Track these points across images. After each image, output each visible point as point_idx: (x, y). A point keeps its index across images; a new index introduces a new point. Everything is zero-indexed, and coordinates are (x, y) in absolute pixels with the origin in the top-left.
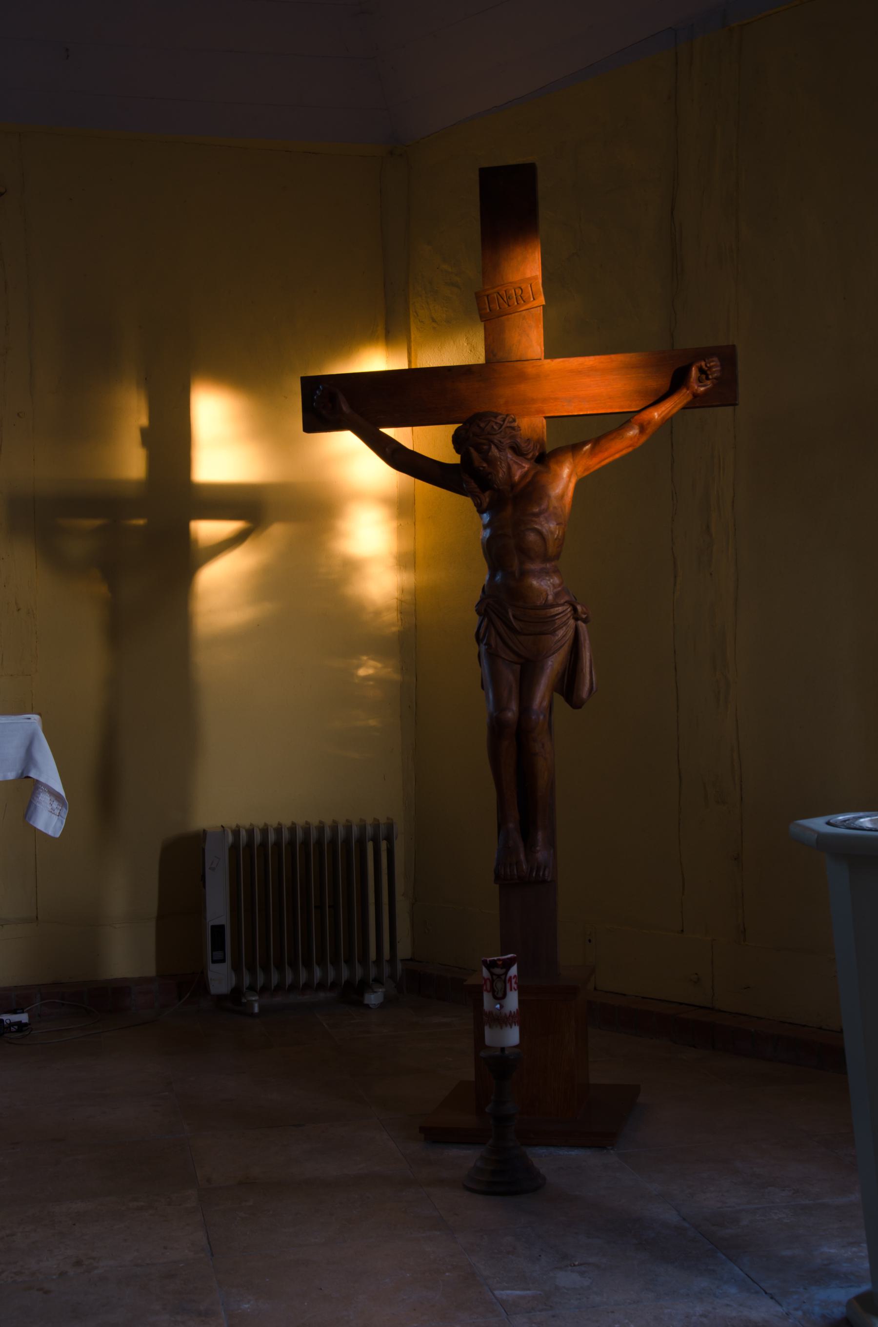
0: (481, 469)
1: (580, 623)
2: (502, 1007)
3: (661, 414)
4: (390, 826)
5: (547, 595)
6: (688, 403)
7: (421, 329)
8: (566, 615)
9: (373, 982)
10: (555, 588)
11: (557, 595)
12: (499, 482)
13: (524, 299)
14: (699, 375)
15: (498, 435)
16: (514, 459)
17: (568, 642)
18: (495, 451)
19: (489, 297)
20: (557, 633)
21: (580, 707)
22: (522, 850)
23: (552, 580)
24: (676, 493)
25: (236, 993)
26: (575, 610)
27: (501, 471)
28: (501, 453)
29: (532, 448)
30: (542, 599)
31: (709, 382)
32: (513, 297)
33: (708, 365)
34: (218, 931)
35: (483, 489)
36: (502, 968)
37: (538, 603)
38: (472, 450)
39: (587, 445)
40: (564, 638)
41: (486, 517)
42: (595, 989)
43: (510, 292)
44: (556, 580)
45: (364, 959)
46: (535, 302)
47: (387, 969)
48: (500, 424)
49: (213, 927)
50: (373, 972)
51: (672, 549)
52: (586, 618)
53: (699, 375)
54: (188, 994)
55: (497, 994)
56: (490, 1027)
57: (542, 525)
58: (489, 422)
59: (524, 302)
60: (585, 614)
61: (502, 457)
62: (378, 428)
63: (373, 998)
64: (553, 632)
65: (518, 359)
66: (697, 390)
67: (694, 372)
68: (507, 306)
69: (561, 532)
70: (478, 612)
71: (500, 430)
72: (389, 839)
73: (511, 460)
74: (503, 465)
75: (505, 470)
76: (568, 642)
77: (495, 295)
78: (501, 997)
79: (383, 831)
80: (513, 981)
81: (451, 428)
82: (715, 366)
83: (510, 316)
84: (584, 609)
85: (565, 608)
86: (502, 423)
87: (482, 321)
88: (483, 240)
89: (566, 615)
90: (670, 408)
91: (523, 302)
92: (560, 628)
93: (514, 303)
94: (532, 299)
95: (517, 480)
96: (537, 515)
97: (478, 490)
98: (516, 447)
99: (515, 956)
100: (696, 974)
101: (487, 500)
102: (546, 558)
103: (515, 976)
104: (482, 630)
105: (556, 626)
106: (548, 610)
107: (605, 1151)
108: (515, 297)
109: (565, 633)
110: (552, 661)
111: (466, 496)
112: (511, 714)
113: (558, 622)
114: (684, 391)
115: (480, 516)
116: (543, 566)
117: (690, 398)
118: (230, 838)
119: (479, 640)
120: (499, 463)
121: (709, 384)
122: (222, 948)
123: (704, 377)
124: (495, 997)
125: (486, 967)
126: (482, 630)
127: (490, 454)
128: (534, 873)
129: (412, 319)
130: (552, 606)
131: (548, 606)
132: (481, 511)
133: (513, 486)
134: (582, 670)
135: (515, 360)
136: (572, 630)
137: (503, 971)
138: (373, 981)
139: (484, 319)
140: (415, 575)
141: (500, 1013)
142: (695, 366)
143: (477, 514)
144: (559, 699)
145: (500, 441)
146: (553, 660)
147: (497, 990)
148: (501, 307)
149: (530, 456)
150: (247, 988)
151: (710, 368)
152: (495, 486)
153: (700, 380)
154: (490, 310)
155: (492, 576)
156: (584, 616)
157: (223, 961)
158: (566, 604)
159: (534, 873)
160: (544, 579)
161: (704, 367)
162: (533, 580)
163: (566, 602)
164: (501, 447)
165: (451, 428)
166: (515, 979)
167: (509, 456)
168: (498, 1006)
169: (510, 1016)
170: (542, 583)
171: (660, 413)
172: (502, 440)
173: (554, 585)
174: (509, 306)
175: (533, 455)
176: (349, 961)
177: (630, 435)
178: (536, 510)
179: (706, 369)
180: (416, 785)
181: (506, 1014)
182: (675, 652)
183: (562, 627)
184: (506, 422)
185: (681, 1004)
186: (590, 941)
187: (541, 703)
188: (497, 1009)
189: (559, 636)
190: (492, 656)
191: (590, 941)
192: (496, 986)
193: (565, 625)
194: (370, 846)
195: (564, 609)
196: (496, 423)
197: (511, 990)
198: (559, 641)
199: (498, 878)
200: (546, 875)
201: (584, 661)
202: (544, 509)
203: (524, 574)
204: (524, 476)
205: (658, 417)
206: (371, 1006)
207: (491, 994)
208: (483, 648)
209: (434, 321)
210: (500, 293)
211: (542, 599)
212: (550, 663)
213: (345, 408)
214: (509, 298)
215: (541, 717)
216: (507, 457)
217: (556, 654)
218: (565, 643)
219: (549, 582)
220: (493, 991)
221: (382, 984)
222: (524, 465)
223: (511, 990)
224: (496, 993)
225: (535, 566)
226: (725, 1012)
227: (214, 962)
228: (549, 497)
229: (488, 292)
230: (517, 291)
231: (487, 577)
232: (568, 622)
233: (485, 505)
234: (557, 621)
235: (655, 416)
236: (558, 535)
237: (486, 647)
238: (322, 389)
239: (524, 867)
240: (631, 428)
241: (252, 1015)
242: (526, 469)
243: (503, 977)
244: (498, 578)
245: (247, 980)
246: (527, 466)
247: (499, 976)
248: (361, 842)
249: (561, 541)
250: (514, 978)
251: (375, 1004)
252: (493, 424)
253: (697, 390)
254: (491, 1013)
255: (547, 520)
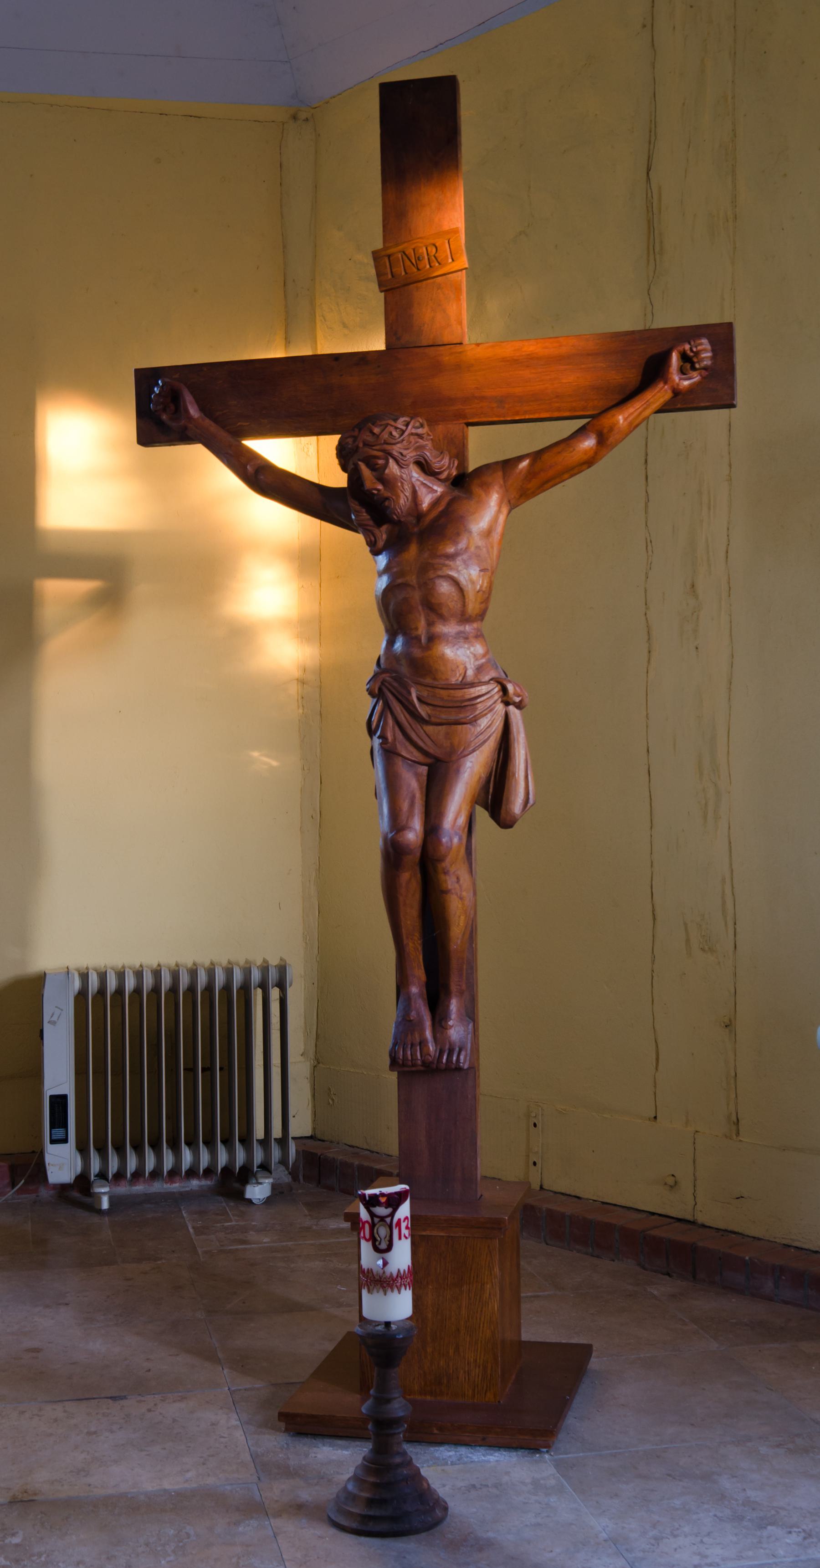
0: (375, 492)
1: (511, 708)
2: (385, 1263)
3: (627, 418)
4: (282, 969)
5: (466, 670)
6: (667, 403)
7: (329, 337)
8: (492, 697)
9: (259, 1169)
10: (477, 660)
11: (479, 669)
12: (399, 510)
13: (439, 260)
14: (682, 364)
15: (399, 445)
16: (421, 479)
17: (494, 735)
18: (393, 467)
19: (391, 259)
20: (479, 722)
21: (510, 826)
22: (428, 1023)
23: (472, 649)
24: (651, 542)
25: (83, 1182)
26: (504, 690)
27: (402, 495)
28: (403, 471)
29: (447, 464)
30: (458, 675)
31: (695, 374)
32: (423, 258)
33: (695, 349)
34: (59, 1102)
35: (379, 524)
36: (386, 1208)
37: (453, 681)
38: (363, 466)
39: (524, 461)
40: (489, 729)
41: (382, 560)
42: (541, 1187)
43: (420, 251)
44: (479, 649)
45: (246, 1140)
46: (454, 264)
47: (276, 1153)
48: (401, 430)
49: (51, 1097)
50: (258, 1156)
51: (646, 614)
52: (521, 701)
53: (682, 364)
54: (23, 1181)
55: (380, 1244)
56: (369, 1291)
57: (458, 571)
58: (386, 427)
59: (440, 264)
60: (518, 696)
61: (404, 476)
62: (239, 439)
63: (258, 1191)
64: (474, 721)
65: (431, 343)
66: (678, 385)
67: (675, 358)
68: (415, 270)
69: (485, 581)
70: (371, 693)
71: (402, 438)
72: (281, 985)
73: (418, 480)
74: (406, 487)
75: (407, 494)
76: (494, 735)
77: (400, 256)
78: (383, 1249)
79: (273, 976)
80: (403, 1225)
81: (334, 439)
82: (705, 350)
83: (419, 284)
84: (517, 689)
85: (490, 687)
86: (404, 428)
87: (381, 291)
88: (384, 181)
89: (492, 697)
90: (640, 410)
91: (437, 264)
92: (482, 715)
93: (425, 266)
94: (450, 260)
95: (425, 509)
96: (452, 557)
97: (371, 523)
98: (423, 461)
99: (407, 1187)
100: (673, 1175)
101: (384, 537)
102: (464, 618)
103: (406, 1218)
104: (375, 718)
105: (478, 712)
106: (466, 690)
107: (537, 1455)
108: (426, 257)
109: (490, 722)
110: (471, 762)
111: (356, 531)
112: (413, 835)
113: (480, 707)
114: (661, 385)
115: (374, 558)
116: (461, 628)
117: (668, 395)
118: (77, 984)
119: (371, 732)
120: (399, 484)
121: (696, 377)
122: (65, 1125)
123: (688, 366)
124: (377, 1249)
125: (364, 1205)
126: (375, 718)
127: (387, 471)
128: (445, 1057)
129: (318, 324)
130: (472, 685)
131: (465, 685)
132: (376, 552)
133: (419, 516)
134: (514, 774)
135: (426, 344)
136: (501, 718)
137: (389, 1211)
138: (258, 1167)
139: (384, 289)
140: (320, 650)
141: (384, 1272)
142: (676, 351)
143: (370, 556)
144: (483, 816)
145: (402, 454)
146: (473, 759)
147: (379, 1239)
148: (407, 272)
149: (444, 476)
150: (96, 1176)
151: (697, 354)
152: (395, 517)
153: (682, 371)
154: (393, 276)
155: (391, 643)
156: (517, 700)
157: (65, 1141)
158: (492, 682)
159: (445, 1057)
160: (461, 647)
161: (689, 352)
162: (446, 647)
163: (491, 680)
164: (401, 461)
165: (334, 439)
166: (406, 1221)
167: (415, 475)
168: (380, 1262)
169: (397, 1276)
170: (459, 652)
171: (626, 415)
172: (404, 452)
173: (475, 656)
174: (418, 269)
175: (449, 475)
176: (227, 1142)
177: (584, 446)
178: (451, 550)
179: (692, 354)
180: (319, 915)
181: (391, 1274)
182: (648, 751)
183: (486, 714)
184: (410, 427)
185: (653, 1214)
186: (535, 1125)
187: (456, 819)
188: (378, 1266)
189: (482, 727)
190: (389, 753)
191: (535, 1125)
192: (378, 1233)
193: (491, 711)
194: (257, 996)
195: (490, 689)
196: (396, 428)
197: (400, 1238)
198: (482, 733)
199: (394, 1063)
200: (462, 1061)
201: (517, 762)
202: (461, 549)
203: (432, 639)
204: (435, 504)
205: (624, 422)
206: (254, 1201)
207: (370, 1243)
208: (377, 742)
209: (345, 326)
210: (407, 253)
211: (458, 675)
212: (468, 764)
213: (194, 411)
214: (418, 259)
215: (456, 840)
216: (411, 477)
217: (477, 752)
218: (489, 737)
219: (468, 652)
220: (373, 1239)
221: (270, 1172)
222: (435, 488)
223: (400, 1238)
224: (377, 1243)
225: (449, 629)
226: (710, 1227)
227: (53, 1142)
228: (470, 532)
229: (390, 251)
230: (429, 249)
231: (384, 644)
232: (495, 707)
233: (381, 544)
234: (479, 705)
235: (619, 420)
236: (481, 587)
237: (381, 741)
238: (161, 384)
239: (431, 1048)
240: (587, 437)
241: (100, 1212)
242: (439, 493)
243: (388, 1220)
244: (398, 645)
245: (95, 1165)
246: (439, 489)
247: (382, 1219)
248: (245, 989)
249: (486, 597)
250: (404, 1221)
251: (259, 1199)
252: (392, 429)
253: (678, 385)
254: (370, 1271)
255: (466, 564)
